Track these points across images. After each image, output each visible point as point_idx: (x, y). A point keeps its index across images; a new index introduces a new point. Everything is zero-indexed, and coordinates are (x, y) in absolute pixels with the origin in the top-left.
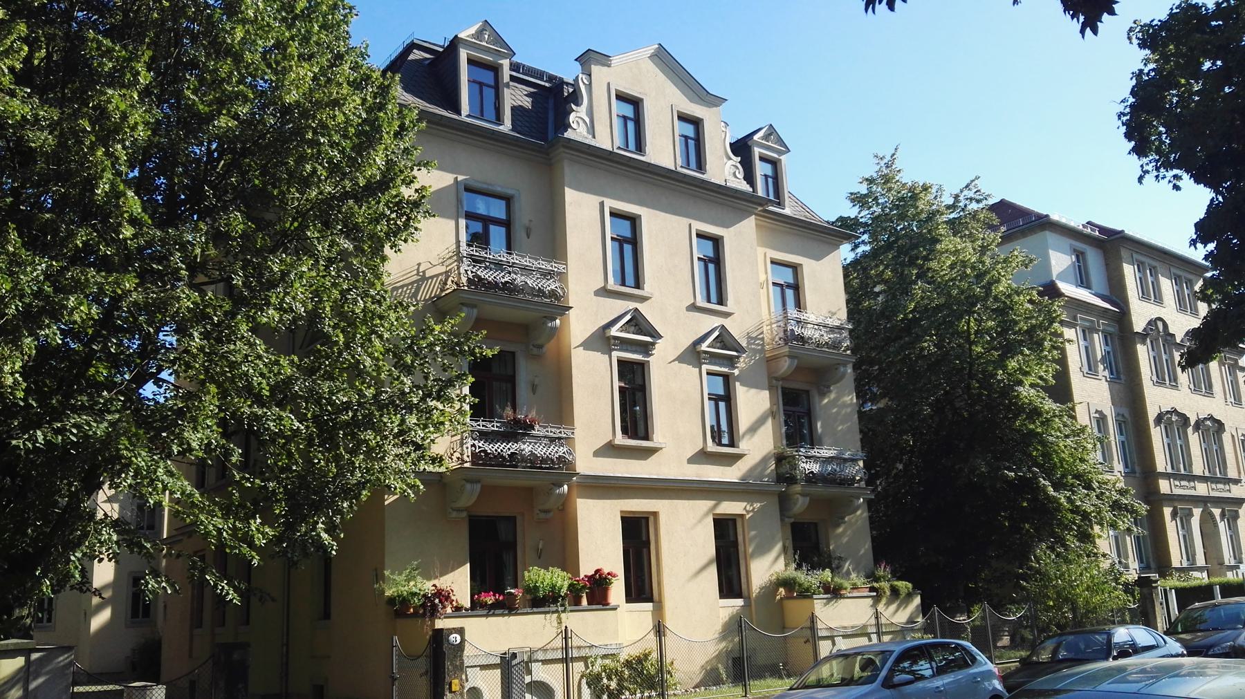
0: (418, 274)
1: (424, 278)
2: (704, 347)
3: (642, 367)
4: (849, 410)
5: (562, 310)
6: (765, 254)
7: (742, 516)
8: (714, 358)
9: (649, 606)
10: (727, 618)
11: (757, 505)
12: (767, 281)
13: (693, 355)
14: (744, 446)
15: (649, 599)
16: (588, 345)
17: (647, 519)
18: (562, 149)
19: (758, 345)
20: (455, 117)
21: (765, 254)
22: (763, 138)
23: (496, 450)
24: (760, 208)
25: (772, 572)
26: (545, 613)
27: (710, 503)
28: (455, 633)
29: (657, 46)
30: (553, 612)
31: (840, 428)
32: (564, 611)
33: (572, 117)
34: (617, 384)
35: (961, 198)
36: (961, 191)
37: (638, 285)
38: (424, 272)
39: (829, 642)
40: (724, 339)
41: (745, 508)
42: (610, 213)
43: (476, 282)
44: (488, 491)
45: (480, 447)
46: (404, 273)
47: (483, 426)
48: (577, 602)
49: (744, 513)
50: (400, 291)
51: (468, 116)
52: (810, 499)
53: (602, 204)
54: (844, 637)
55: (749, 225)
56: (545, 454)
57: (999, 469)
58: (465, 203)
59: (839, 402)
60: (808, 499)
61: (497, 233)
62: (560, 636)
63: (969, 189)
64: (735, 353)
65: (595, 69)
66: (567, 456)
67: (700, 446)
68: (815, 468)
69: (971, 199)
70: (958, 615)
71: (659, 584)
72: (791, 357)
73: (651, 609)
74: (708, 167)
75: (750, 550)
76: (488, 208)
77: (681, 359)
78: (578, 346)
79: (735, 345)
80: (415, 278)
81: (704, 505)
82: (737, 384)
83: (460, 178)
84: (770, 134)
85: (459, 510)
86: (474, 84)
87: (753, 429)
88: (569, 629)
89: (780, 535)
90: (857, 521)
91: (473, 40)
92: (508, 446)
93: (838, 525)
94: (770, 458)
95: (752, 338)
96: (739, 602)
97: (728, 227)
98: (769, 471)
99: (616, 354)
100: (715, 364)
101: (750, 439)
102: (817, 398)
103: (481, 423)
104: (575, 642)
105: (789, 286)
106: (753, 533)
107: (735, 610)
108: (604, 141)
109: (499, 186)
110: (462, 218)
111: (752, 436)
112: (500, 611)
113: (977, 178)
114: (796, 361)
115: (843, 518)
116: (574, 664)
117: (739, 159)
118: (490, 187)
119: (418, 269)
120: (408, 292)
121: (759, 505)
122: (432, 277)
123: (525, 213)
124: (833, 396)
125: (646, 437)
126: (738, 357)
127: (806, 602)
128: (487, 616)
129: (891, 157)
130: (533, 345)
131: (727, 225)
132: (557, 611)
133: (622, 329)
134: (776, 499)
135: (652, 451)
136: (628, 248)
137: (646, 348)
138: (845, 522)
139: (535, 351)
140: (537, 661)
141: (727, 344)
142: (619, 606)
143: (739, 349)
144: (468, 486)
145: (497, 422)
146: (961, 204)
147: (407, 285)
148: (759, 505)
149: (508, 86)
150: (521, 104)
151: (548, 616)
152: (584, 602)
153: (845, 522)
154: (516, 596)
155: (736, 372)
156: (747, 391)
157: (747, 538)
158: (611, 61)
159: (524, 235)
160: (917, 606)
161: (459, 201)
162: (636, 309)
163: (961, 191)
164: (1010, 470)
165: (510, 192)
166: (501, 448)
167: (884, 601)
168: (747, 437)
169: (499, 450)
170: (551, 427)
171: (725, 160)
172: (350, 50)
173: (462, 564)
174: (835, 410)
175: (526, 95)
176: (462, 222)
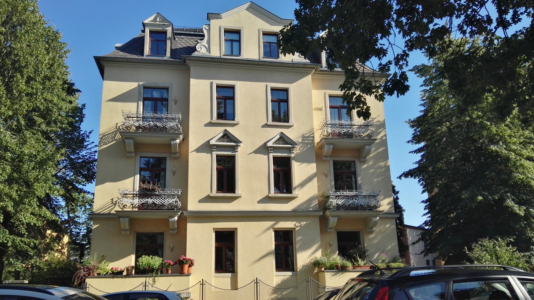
0: (116, 128)
3: (232, 158)
5: (373, 141)
6: (325, 93)
7: (295, 228)
8: (275, 149)
10: (280, 282)
11: (303, 223)
14: (295, 193)
19: (310, 140)
21: (325, 93)
25: (312, 257)
27: (271, 223)
29: (250, 3)
30: (150, 277)
32: (156, 276)
40: (283, 139)
41: (295, 225)
42: (329, 96)
46: (109, 128)
47: (349, 193)
49: (294, 227)
50: (107, 136)
52: (338, 219)
53: (212, 83)
60: (336, 218)
66: (174, 203)
67: (266, 194)
68: (340, 202)
73: (231, 276)
77: (256, 152)
78: (193, 151)
79: (236, 140)
80: (115, 130)
83: (141, 83)
87: (303, 185)
89: (320, 238)
91: (152, 23)
93: (371, 232)
95: (306, 137)
96: (290, 273)
98: (313, 205)
99: (215, 153)
100: (222, 151)
101: (299, 190)
102: (358, 164)
103: (348, 192)
107: (286, 278)
108: (215, 53)
109: (161, 84)
110: (141, 101)
119: (116, 126)
120: (111, 136)
121: (305, 223)
123: (173, 94)
128: (113, 277)
132: (152, 276)
133: (217, 141)
134: (318, 220)
137: (234, 148)
138: (374, 231)
139: (363, 159)
141: (287, 141)
143: (293, 143)
147: (110, 133)
148: (305, 223)
152: (170, 271)
155: (293, 155)
159: (173, 103)
161: (140, 93)
162: (226, 130)
165: (166, 85)
166: (342, 202)
172: (405, 60)
173: (335, 253)
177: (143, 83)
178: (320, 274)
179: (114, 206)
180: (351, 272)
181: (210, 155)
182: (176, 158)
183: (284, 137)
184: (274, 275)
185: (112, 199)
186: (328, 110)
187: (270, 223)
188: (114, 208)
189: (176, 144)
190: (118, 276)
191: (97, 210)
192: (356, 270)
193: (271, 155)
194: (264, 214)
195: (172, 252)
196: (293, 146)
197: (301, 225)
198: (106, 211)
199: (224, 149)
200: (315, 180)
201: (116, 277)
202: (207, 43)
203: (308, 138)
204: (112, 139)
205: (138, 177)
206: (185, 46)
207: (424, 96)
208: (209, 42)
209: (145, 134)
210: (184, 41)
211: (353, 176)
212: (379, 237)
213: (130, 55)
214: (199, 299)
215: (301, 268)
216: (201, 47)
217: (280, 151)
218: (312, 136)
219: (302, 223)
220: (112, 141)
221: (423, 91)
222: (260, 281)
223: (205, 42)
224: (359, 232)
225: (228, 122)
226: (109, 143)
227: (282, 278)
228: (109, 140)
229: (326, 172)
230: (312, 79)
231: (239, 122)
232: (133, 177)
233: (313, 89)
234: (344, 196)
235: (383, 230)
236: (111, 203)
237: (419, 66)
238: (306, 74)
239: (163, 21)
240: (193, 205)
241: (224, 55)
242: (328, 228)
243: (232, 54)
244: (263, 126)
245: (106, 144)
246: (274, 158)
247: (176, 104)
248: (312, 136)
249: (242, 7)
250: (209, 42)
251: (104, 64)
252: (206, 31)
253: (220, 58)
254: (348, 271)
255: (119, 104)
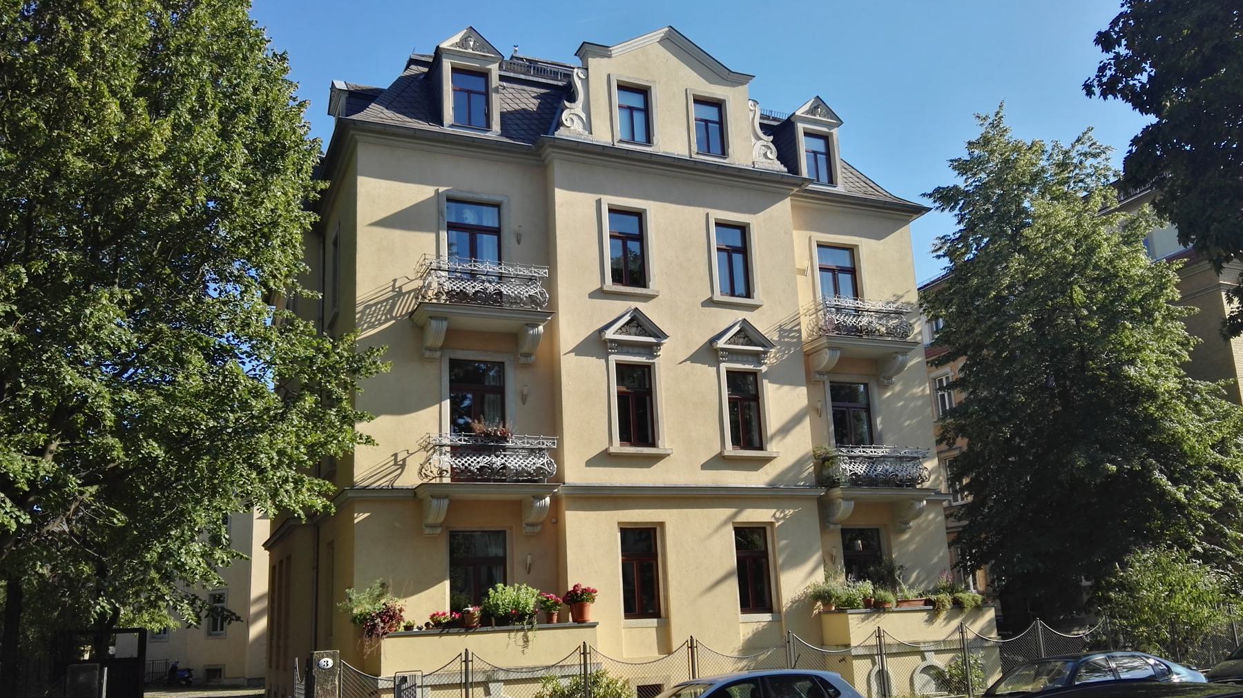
0: (393, 290)
1: (400, 294)
2: (721, 344)
4: (920, 403)
6: (810, 237)
7: (771, 524)
8: (732, 355)
9: (653, 622)
10: (750, 634)
11: (789, 512)
12: (812, 266)
13: (709, 353)
14: (772, 448)
15: (657, 615)
16: (580, 350)
17: (655, 529)
18: (549, 150)
19: (793, 337)
20: (436, 128)
21: (810, 237)
22: (808, 112)
23: (463, 465)
24: (796, 189)
25: (808, 583)
26: (510, 631)
27: (728, 512)
28: (327, 657)
29: (667, 29)
30: (518, 631)
31: (907, 423)
33: (565, 115)
34: (614, 389)
35: (1073, 154)
36: (1073, 146)
37: (748, 294)
38: (400, 288)
39: (869, 661)
40: (746, 333)
42: (716, 223)
43: (462, 296)
44: (455, 506)
45: (851, 471)
46: (378, 290)
48: (550, 620)
49: (773, 520)
50: (374, 308)
51: (452, 126)
53: (599, 202)
54: (937, 652)
55: (783, 208)
56: (519, 466)
57: (1102, 462)
58: (446, 215)
59: (907, 395)
60: (853, 502)
61: (487, 242)
62: (578, 651)
63: (1082, 143)
64: (760, 349)
65: (593, 62)
66: (547, 468)
67: (605, 445)
68: (861, 469)
69: (1085, 154)
70: (1077, 628)
71: (666, 599)
72: (832, 348)
73: (656, 625)
74: (730, 151)
75: (780, 561)
76: (480, 218)
77: (695, 358)
78: (569, 352)
80: (391, 294)
81: (723, 513)
82: (765, 382)
83: (442, 189)
84: (816, 107)
85: (433, 526)
86: (459, 93)
87: (785, 430)
88: (881, 629)
89: (819, 544)
90: (928, 526)
91: (458, 49)
92: (478, 460)
93: (903, 531)
94: (807, 461)
95: (786, 331)
96: (767, 617)
97: (755, 213)
98: (806, 474)
99: (613, 359)
100: (627, 353)
101: (781, 440)
102: (875, 391)
103: (873, 450)
104: (476, 665)
105: (843, 270)
106: (783, 542)
108: (602, 135)
110: (443, 229)
111: (784, 438)
112: (456, 630)
113: (1090, 129)
114: (838, 353)
115: (908, 523)
116: (475, 689)
117: (771, 138)
118: (475, 196)
119: (394, 286)
120: (382, 309)
121: (792, 511)
122: (409, 292)
123: (514, 220)
124: (898, 388)
125: (653, 445)
126: (765, 353)
127: (840, 616)
128: (440, 634)
129: (996, 115)
130: (521, 355)
131: (754, 211)
132: (522, 630)
134: (814, 506)
135: (659, 458)
136: (737, 258)
137: (651, 350)
138: (910, 528)
140: (498, 681)
141: (752, 339)
142: (598, 623)
143: (767, 344)
144: (435, 502)
145: (465, 436)
146: (1075, 161)
147: (381, 302)
148: (792, 511)
149: (496, 90)
150: (524, 106)
151: (513, 634)
153: (910, 528)
154: (473, 614)
155: (764, 369)
156: (778, 388)
157: (778, 548)
158: (611, 51)
159: (514, 241)
160: (990, 621)
161: (440, 213)
162: (636, 309)
163: (1073, 146)
164: (1113, 462)
167: (943, 615)
168: (778, 438)
169: (467, 465)
170: (528, 438)
171: (753, 140)
174: (900, 404)
175: (533, 97)
176: (444, 235)
177: (446, 188)
178: (826, 618)
179: (399, 471)
180: (893, 612)
181: (603, 361)
182: (526, 366)
183: (639, 317)
184: (740, 621)
185: (395, 455)
186: (817, 273)
187: (724, 513)
188: (400, 475)
189: (539, 335)
190: (452, 630)
191: (364, 480)
192: (902, 609)
193: (724, 367)
194: (724, 493)
195: (529, 573)
196: (766, 349)
197: (785, 515)
198: (383, 483)
199: (631, 350)
200: (807, 422)
201: (448, 634)
202: (583, 110)
203: (788, 332)
204: (386, 317)
205: (447, 404)
206: (517, 107)
207: (940, 248)
208: (587, 108)
209: (492, 312)
210: (511, 96)
211: (864, 415)
212: (918, 539)
213: (410, 120)
214: (459, 695)
215: (788, 605)
216: (572, 119)
217: (740, 358)
218: (797, 328)
219: (787, 512)
220: (386, 321)
221: (941, 239)
222: (592, 651)
223: (578, 107)
224: (877, 530)
225: (637, 292)
226: (380, 324)
227: (755, 626)
228: (379, 317)
229: (819, 405)
230: (793, 206)
231: (658, 292)
232: (438, 406)
233: (795, 229)
234: (865, 457)
235: (925, 524)
236: (392, 463)
237: (944, 188)
238: (782, 197)
239: (481, 48)
240: (576, 473)
241: (621, 141)
242: (829, 522)
243: (632, 140)
244: (705, 304)
245: (373, 326)
246: (730, 373)
247: (519, 244)
248: (797, 328)
249: (652, 36)
250: (587, 108)
251: (357, 137)
252: (580, 82)
253: (613, 148)
254: (889, 612)
255: (397, 234)
